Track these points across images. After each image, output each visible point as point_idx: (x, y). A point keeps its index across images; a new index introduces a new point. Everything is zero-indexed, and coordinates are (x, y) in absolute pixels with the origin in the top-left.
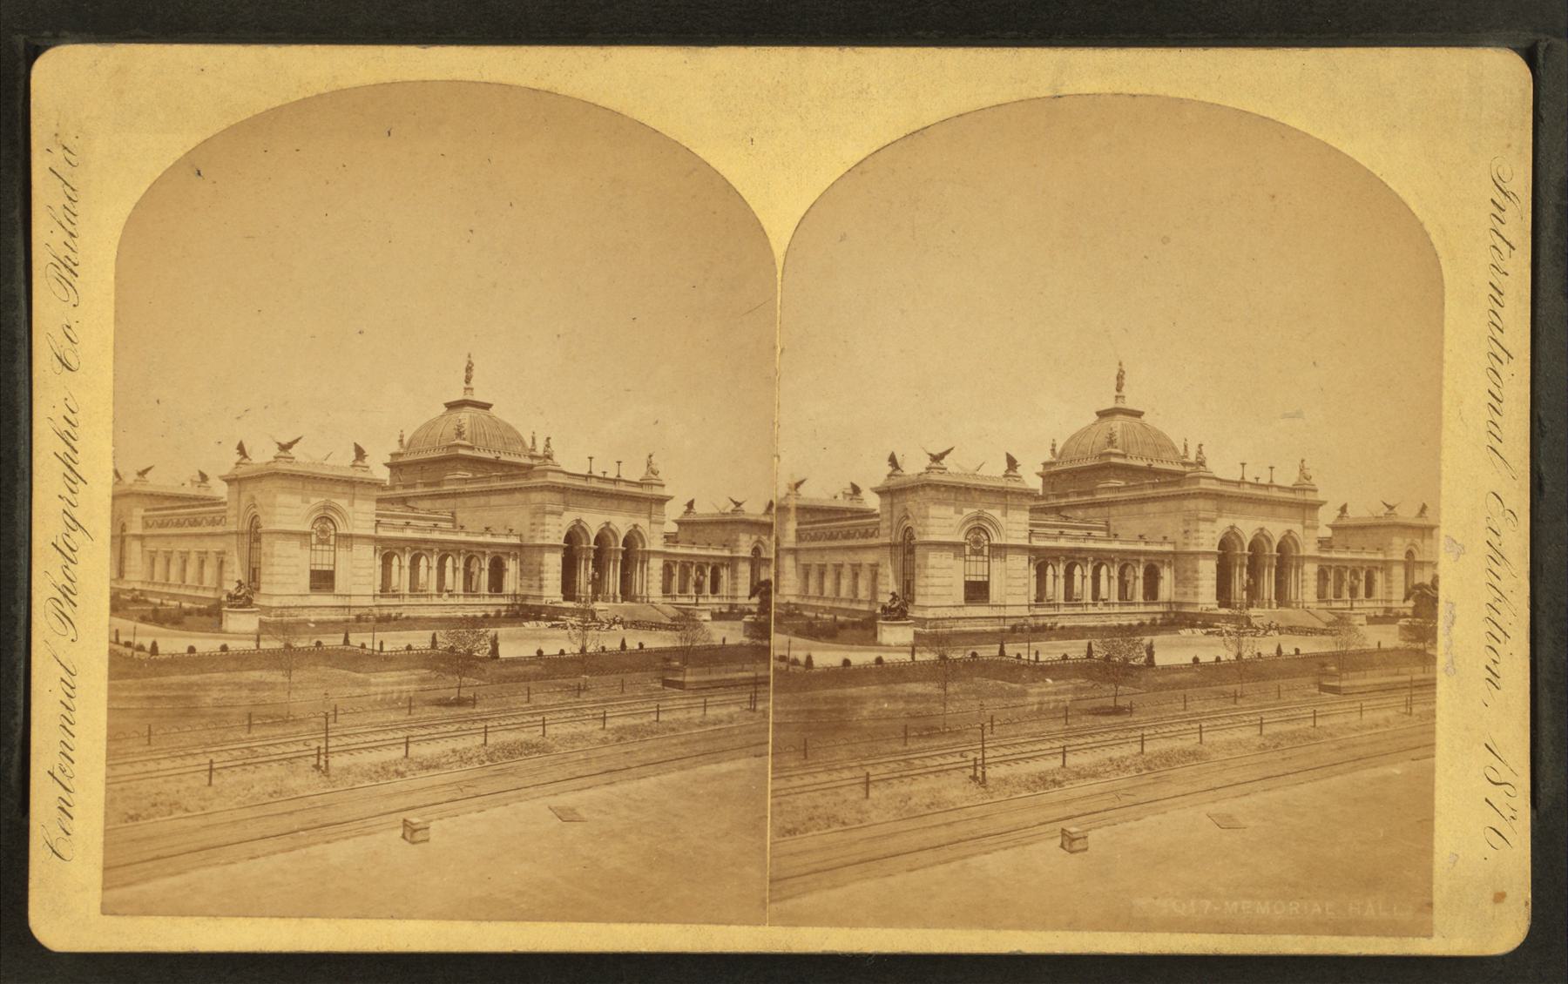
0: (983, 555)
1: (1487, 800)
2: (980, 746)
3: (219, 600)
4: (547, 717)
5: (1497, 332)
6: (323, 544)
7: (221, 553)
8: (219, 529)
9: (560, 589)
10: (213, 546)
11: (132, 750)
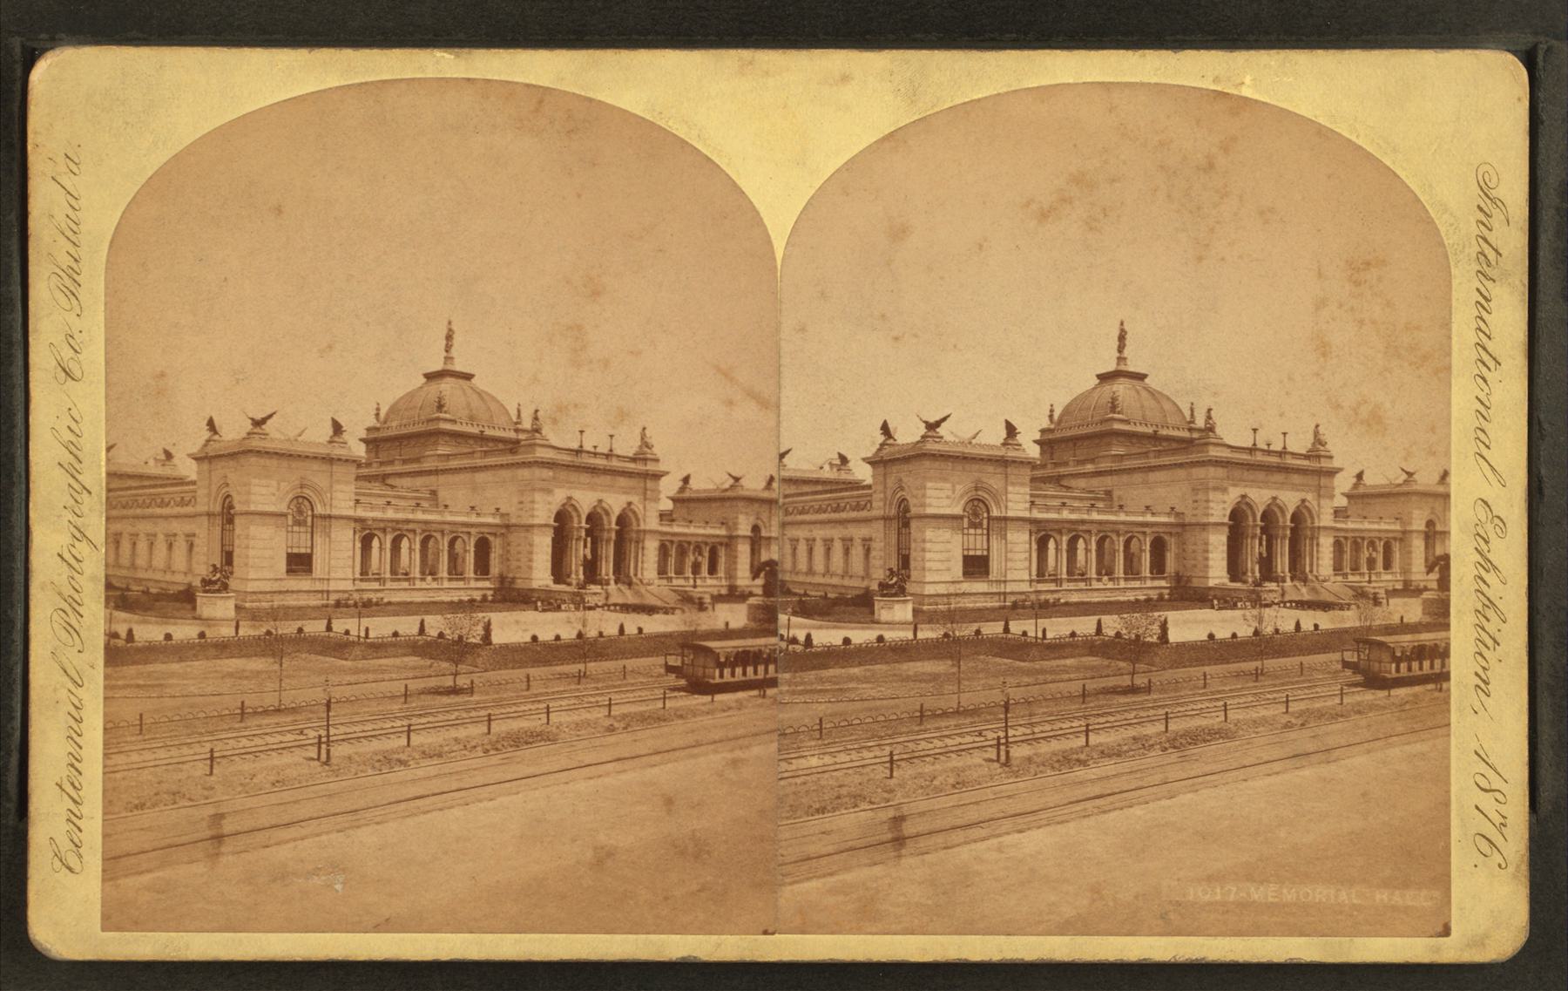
1: (1477, 808)
2: (325, 723)
3: (867, 589)
4: (1228, 703)
6: (976, 528)
7: (190, 536)
8: (189, 510)
9: (549, 572)
10: (858, 532)
11: (125, 739)
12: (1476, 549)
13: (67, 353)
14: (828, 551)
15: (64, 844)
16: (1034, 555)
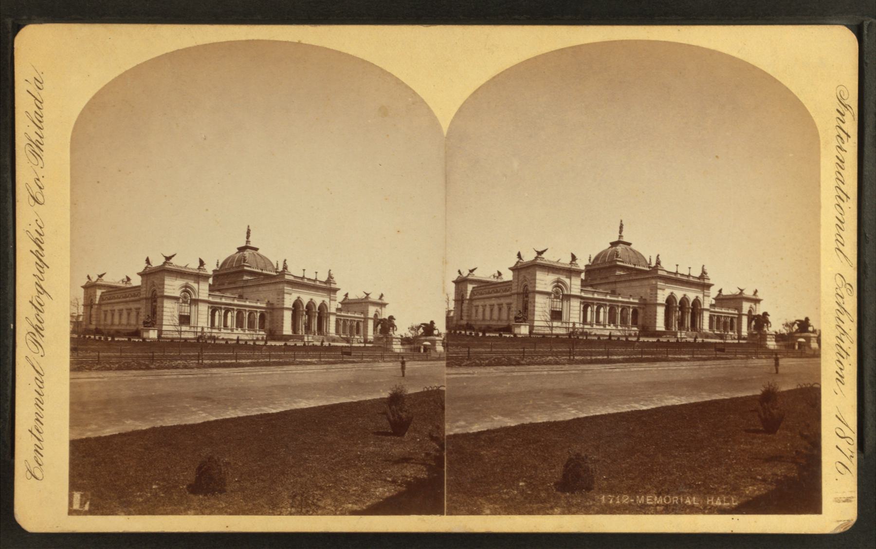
0: (188, 304)
1: (837, 447)
5: (840, 183)
7: (509, 304)
12: (836, 302)
13: (35, 189)
14: (500, 309)
15: (33, 464)
16: (210, 317)
